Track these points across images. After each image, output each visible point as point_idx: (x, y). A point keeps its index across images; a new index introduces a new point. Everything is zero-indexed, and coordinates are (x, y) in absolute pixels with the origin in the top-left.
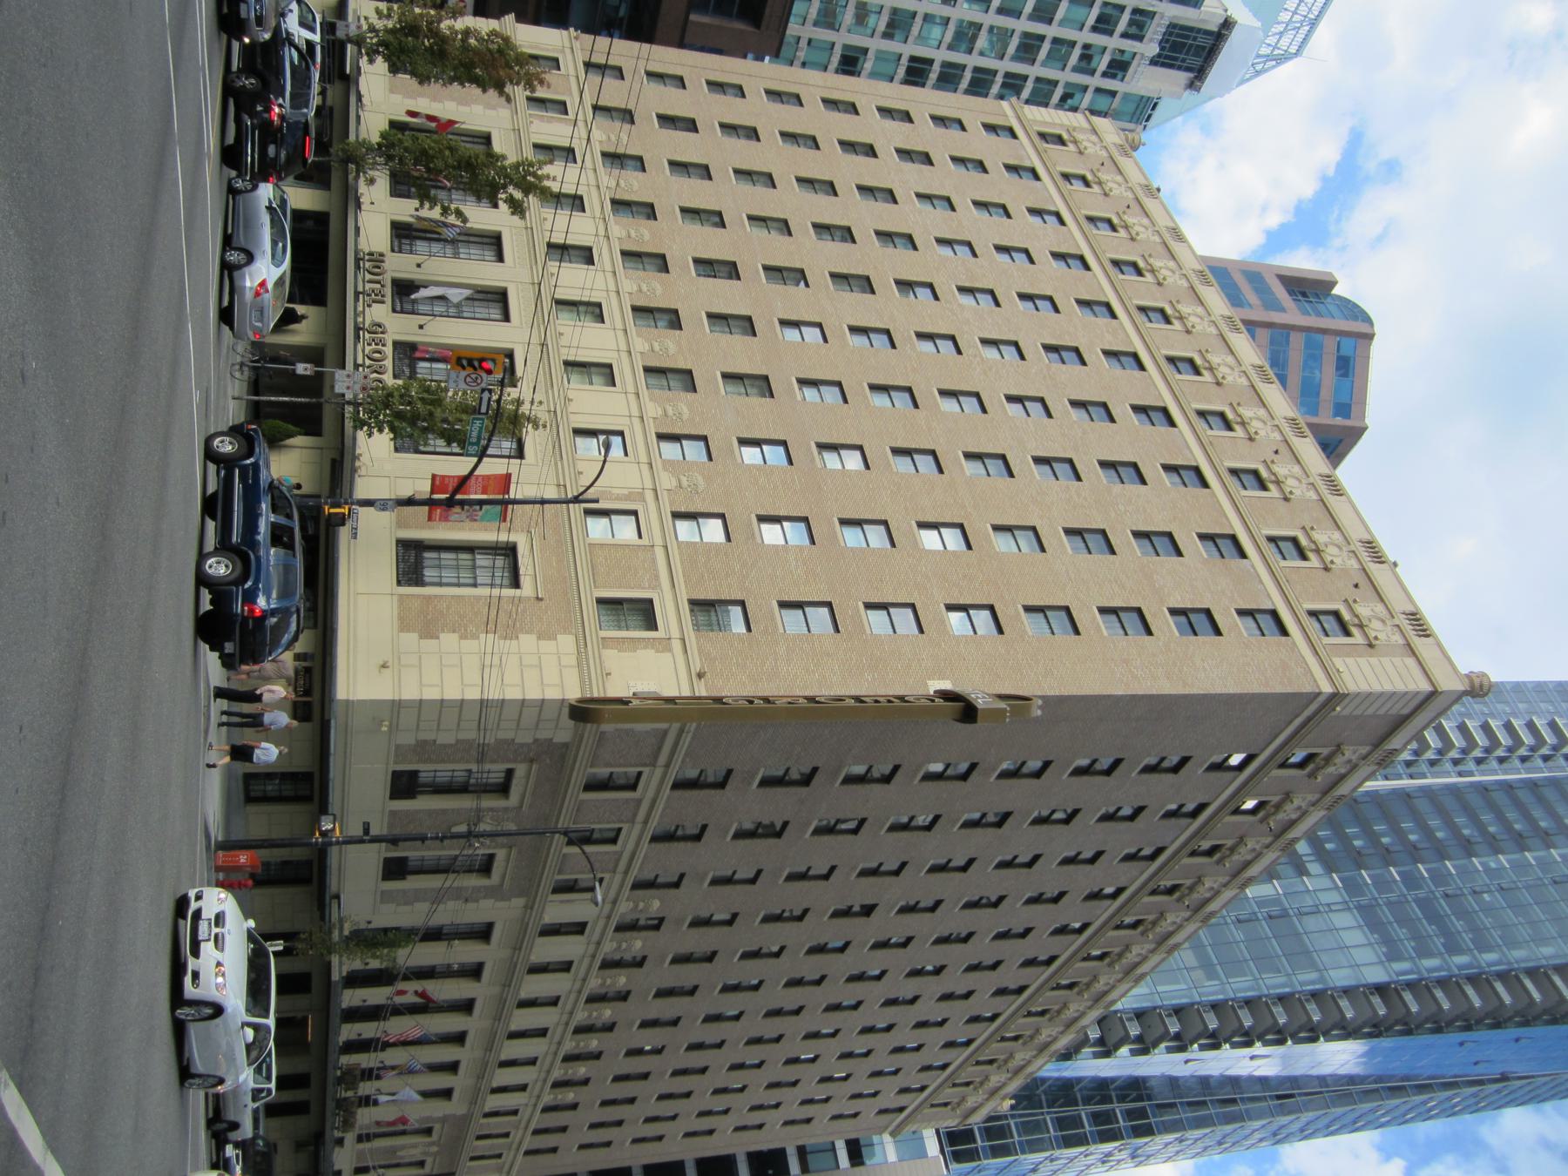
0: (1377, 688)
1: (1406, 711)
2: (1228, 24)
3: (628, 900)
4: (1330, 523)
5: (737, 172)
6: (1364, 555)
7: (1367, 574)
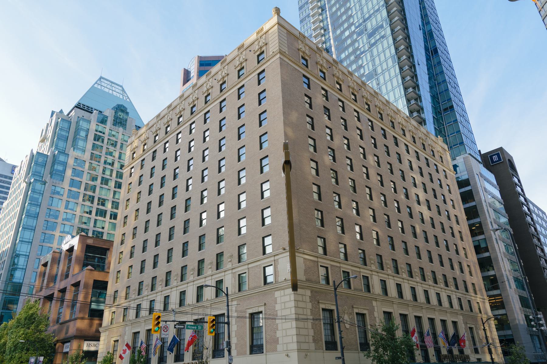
0: (277, 41)
1: (285, 31)
3: (440, 285)
4: (234, 61)
5: (143, 252)
6: (242, 50)
7: (247, 48)
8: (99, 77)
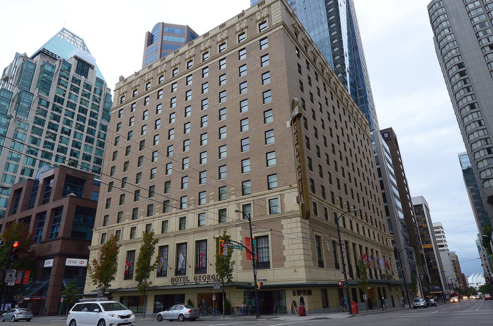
2: (76, 57)
8: (61, 28)
